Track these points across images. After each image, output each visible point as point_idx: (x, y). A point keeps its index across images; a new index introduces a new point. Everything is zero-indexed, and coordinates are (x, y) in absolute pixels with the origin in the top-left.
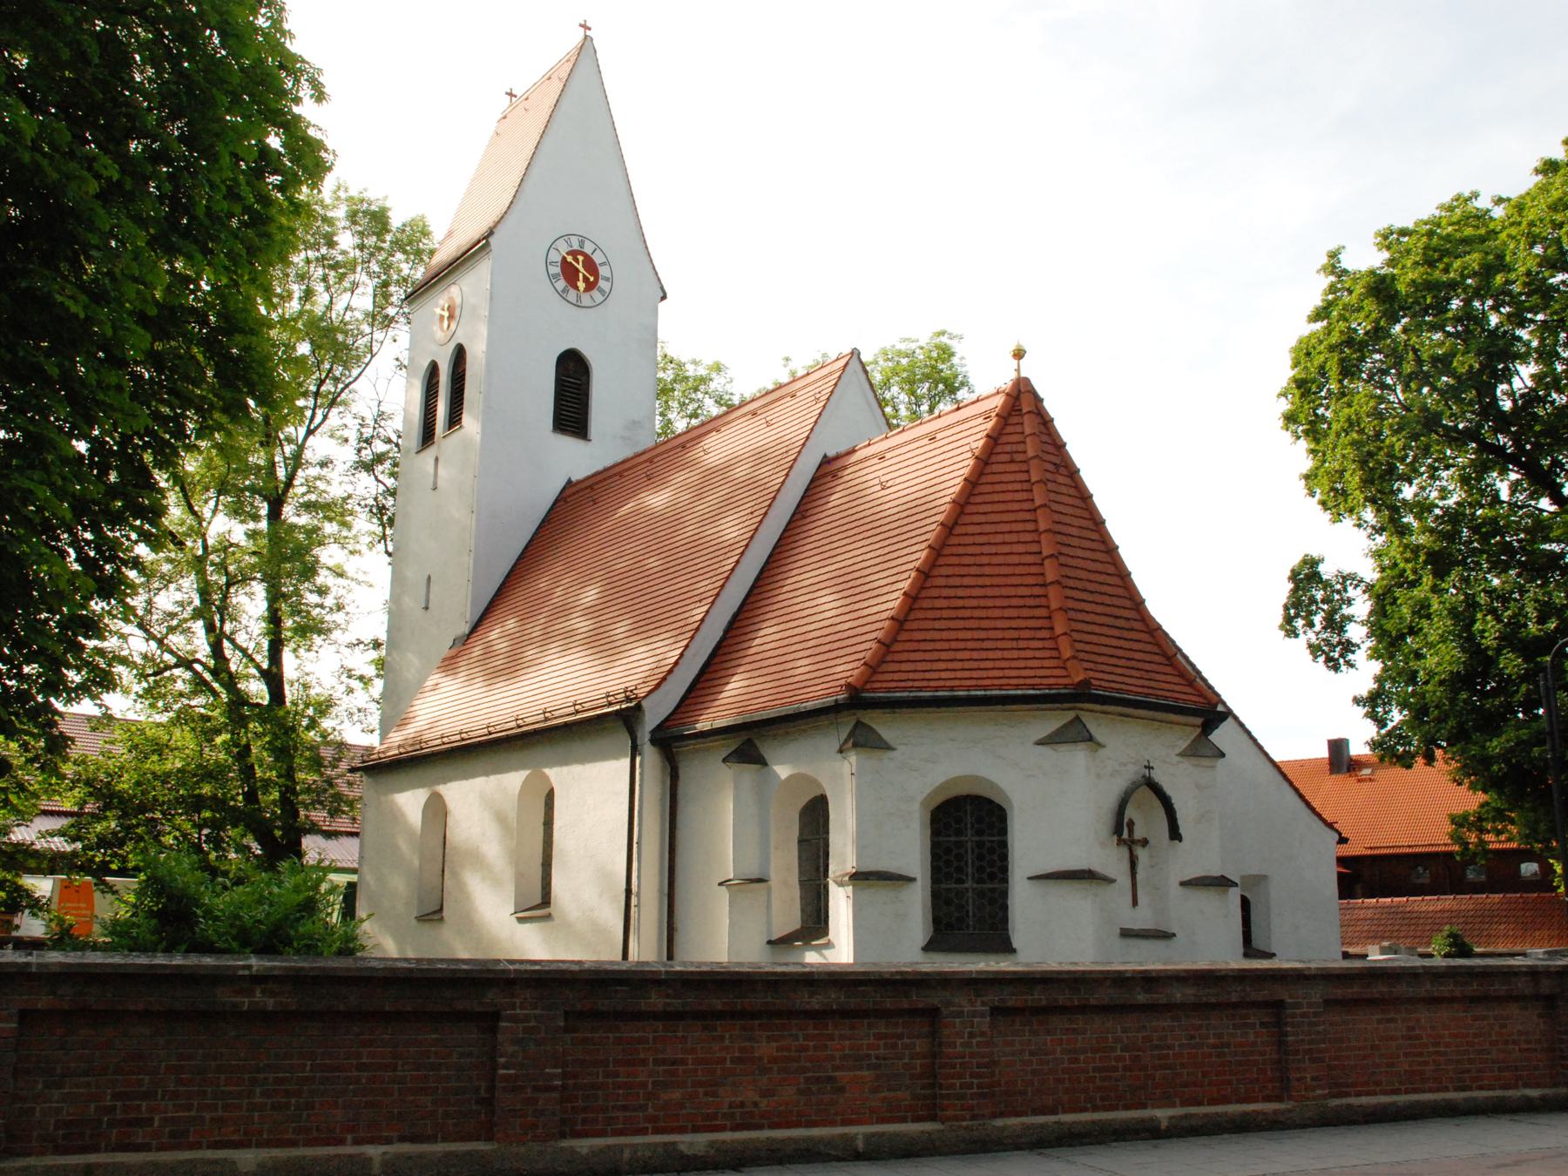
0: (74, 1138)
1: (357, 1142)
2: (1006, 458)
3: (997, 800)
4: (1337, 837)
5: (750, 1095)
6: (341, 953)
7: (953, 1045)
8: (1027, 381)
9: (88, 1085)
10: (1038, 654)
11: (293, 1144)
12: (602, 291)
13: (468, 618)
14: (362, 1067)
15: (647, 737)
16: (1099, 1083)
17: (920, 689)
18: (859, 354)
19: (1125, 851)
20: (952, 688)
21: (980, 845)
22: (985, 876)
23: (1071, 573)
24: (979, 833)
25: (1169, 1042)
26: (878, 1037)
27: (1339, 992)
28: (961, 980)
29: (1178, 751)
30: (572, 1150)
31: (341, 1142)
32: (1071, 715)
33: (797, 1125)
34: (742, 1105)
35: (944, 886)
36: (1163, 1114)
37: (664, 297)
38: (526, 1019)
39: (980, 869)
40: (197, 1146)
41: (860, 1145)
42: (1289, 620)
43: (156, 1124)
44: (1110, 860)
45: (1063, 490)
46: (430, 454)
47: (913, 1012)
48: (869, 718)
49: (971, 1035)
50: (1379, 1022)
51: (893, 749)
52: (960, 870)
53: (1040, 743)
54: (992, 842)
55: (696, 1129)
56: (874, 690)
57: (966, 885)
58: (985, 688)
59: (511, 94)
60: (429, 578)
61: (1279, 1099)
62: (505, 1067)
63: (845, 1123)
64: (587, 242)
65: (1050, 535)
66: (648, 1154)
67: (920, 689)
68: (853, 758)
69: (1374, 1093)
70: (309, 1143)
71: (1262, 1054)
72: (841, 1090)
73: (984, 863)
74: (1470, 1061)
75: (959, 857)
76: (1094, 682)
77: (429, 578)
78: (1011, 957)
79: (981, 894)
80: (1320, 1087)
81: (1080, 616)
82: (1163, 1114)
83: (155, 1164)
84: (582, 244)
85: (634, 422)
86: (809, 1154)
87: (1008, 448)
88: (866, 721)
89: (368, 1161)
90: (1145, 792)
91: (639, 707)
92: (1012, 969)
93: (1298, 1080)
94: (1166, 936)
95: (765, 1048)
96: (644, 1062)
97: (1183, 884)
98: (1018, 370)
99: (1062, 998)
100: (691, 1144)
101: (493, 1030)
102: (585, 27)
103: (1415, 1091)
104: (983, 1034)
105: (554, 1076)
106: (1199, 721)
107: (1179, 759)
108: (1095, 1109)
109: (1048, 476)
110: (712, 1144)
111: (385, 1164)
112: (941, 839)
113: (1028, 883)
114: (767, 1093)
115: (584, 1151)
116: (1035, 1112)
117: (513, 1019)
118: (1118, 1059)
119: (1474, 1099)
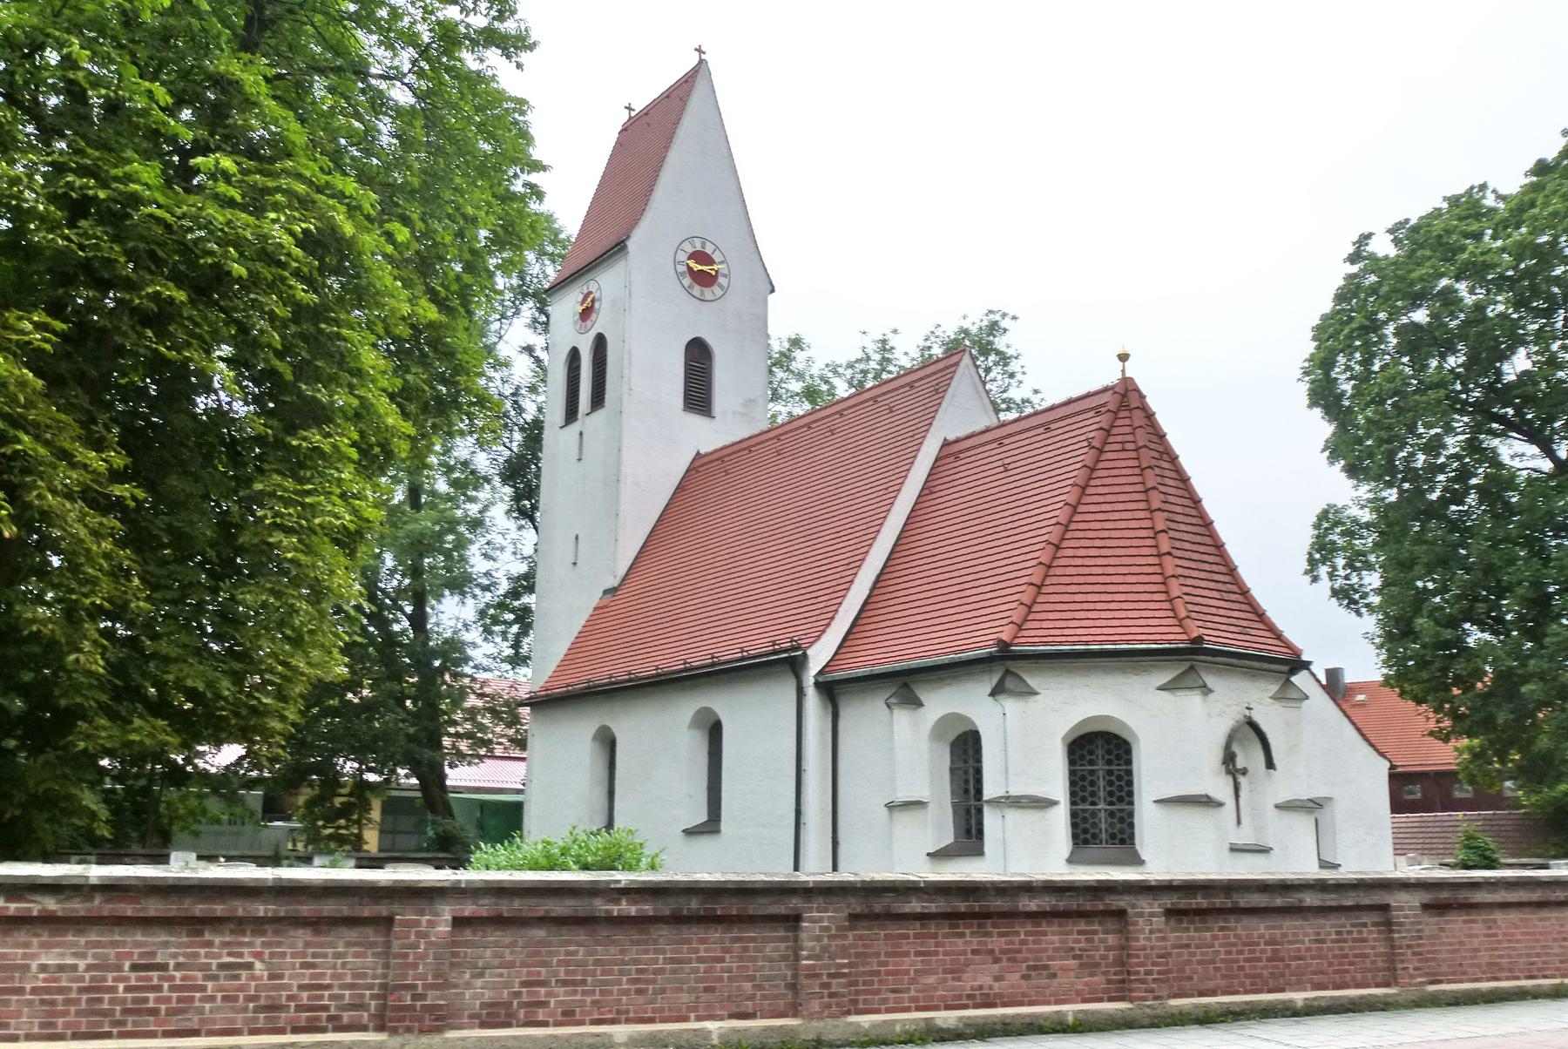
0: (495, 1016)
1: (699, 1019)
2: (1119, 447)
3: (1124, 735)
4: (1388, 765)
5: (986, 980)
6: (653, 867)
7: (1137, 940)
8: (1131, 379)
9: (501, 975)
11: (651, 1020)
12: (721, 286)
14: (700, 960)
15: (811, 681)
16: (1248, 971)
17: (1060, 643)
19: (1230, 779)
20: (1087, 643)
21: (1110, 773)
22: (1114, 799)
23: (1178, 544)
25: (1301, 938)
26: (1079, 933)
29: (1271, 694)
30: (858, 1024)
31: (686, 1019)
32: (1186, 665)
33: (1021, 1004)
34: (981, 988)
35: (1081, 807)
36: (1298, 997)
37: (773, 291)
38: (821, 920)
39: (1111, 794)
40: (581, 1023)
41: (1070, 1019)
42: (1313, 563)
43: (552, 1005)
44: (1219, 787)
45: (1167, 473)
46: (575, 428)
48: (1014, 666)
49: (1151, 932)
50: (1465, 922)
52: (1093, 794)
53: (1161, 688)
55: (948, 1008)
58: (1114, 642)
59: (629, 108)
60: (577, 537)
61: (1387, 985)
62: (807, 958)
63: (1058, 1002)
64: (708, 244)
66: (913, 1027)
69: (1461, 981)
70: (664, 1020)
71: (1373, 948)
72: (1054, 976)
73: (1090, 789)
74: (1538, 955)
75: (1092, 783)
76: (1206, 638)
77: (577, 537)
78: (1140, 869)
79: (1112, 814)
80: (1420, 976)
81: (1189, 582)
82: (1298, 997)
83: (555, 1037)
84: (703, 245)
85: (750, 400)
86: (1008, 1030)
87: (1119, 439)
89: (706, 1034)
90: (1248, 729)
91: (805, 656)
92: (664, 879)
93: (1404, 969)
94: (1265, 850)
95: (996, 942)
96: (907, 954)
97: (1277, 807)
98: (1123, 371)
99: (1218, 901)
100: (945, 1019)
101: (796, 928)
102: (699, 50)
103: (1496, 979)
104: (1160, 931)
105: (844, 966)
106: (1285, 668)
108: (1246, 992)
109: (1154, 462)
110: (960, 1019)
111: (721, 1036)
112: (1124, 767)
113: (1154, 806)
114: (998, 979)
115: (867, 1026)
116: (1201, 994)
117: (812, 920)
118: (1263, 951)
119: (1539, 986)
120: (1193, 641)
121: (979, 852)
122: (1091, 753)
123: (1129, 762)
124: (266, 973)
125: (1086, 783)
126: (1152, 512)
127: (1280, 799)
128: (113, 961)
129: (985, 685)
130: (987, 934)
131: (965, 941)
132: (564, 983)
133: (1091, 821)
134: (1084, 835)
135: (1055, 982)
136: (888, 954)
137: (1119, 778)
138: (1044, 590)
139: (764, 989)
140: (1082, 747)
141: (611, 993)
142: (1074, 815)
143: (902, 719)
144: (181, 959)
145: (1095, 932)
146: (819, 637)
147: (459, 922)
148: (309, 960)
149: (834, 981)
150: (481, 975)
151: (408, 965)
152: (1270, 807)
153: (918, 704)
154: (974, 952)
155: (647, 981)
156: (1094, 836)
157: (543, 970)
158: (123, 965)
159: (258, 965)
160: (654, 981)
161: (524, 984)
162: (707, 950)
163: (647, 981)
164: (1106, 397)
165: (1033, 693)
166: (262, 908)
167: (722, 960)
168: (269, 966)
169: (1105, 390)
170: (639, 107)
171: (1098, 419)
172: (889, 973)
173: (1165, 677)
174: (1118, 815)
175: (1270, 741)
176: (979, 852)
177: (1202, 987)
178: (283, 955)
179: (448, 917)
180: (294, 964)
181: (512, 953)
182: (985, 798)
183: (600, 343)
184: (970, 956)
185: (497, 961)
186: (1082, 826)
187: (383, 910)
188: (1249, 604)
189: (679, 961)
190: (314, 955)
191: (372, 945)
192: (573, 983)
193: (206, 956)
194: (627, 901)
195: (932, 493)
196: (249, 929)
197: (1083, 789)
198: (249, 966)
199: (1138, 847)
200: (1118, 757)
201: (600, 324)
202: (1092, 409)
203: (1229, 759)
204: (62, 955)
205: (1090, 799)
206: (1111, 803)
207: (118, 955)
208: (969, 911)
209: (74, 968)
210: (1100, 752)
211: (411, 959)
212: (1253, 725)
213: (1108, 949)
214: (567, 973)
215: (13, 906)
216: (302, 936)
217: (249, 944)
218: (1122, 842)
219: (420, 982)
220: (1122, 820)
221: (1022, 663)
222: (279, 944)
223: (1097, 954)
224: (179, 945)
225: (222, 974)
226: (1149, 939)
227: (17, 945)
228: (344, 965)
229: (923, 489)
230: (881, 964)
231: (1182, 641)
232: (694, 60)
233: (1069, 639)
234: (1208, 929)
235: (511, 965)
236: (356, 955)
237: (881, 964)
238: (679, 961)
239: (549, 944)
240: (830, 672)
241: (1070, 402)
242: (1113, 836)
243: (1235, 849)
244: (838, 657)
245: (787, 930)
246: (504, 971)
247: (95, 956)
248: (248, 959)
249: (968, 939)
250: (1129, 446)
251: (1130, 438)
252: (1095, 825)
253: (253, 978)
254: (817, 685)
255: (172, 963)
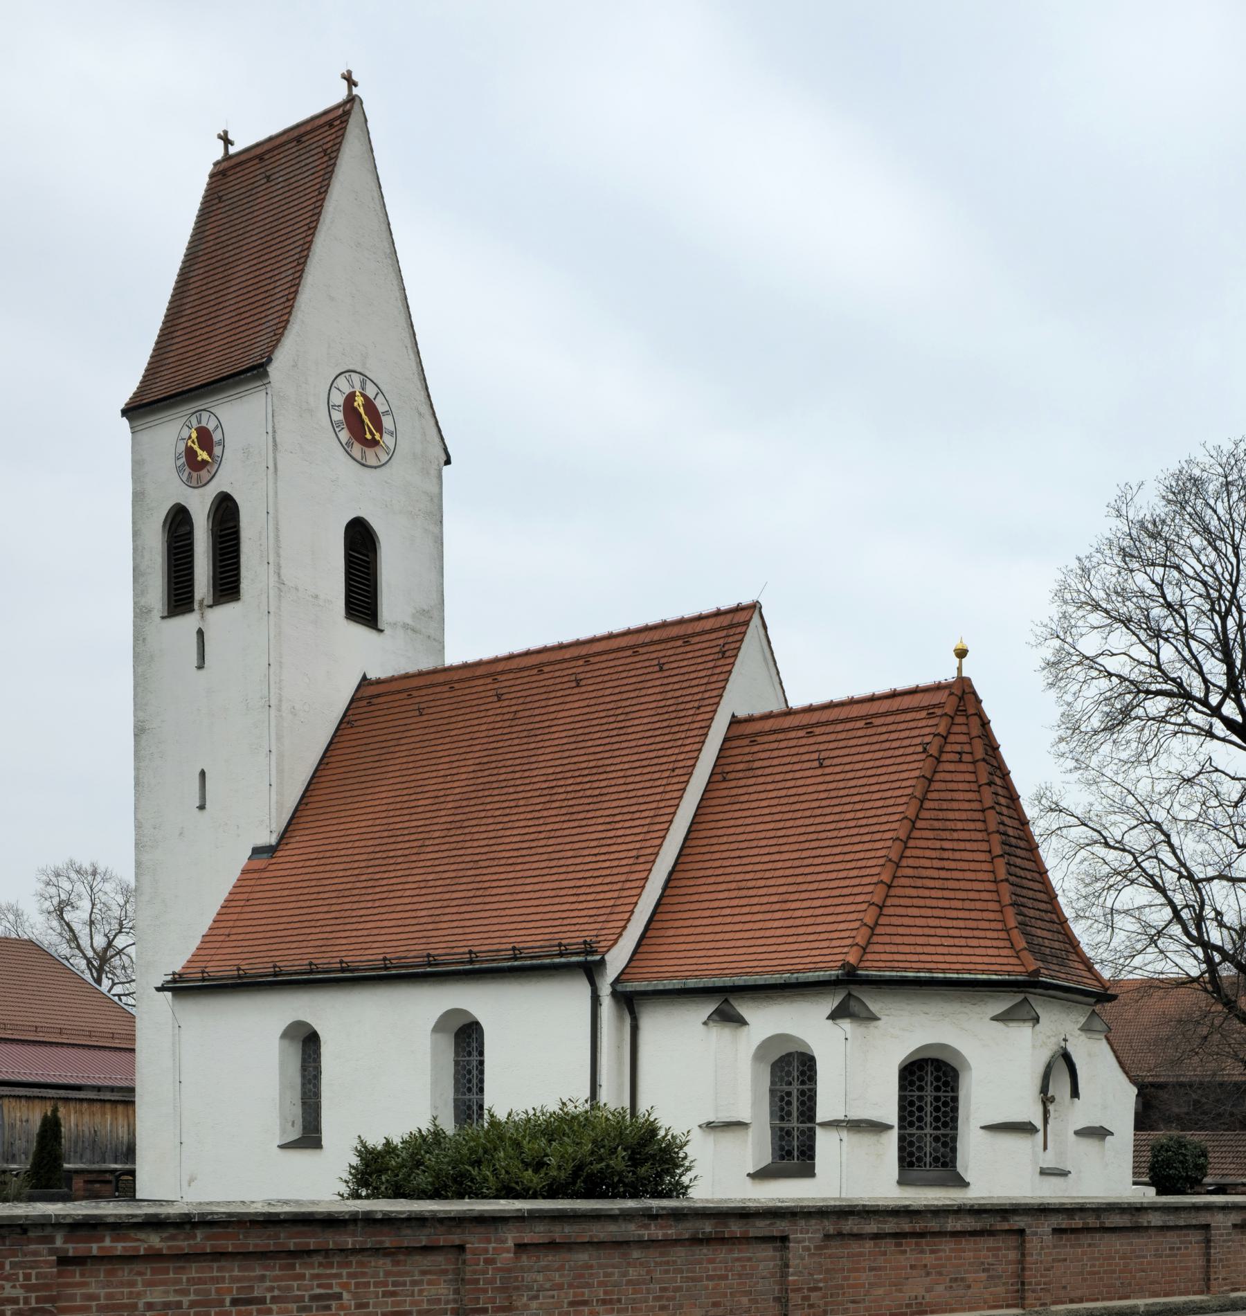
10: (995, 943)
12: (199, 478)
13: (274, 827)
14: (710, 1278)
17: (905, 969)
18: (761, 608)
20: (930, 971)
21: (937, 1099)
22: (940, 1124)
24: (937, 1089)
26: (989, 1249)
27: (1065, 1223)
28: (1024, 1209)
32: (1020, 997)
35: (942, 1132)
37: (448, 462)
38: (803, 1240)
39: (937, 1119)
46: (187, 624)
47: (1196, 1227)
48: (856, 991)
49: (1042, 1248)
51: (879, 1019)
52: (920, 1119)
53: (995, 1019)
54: (945, 1091)
56: (866, 968)
57: (925, 1131)
58: (958, 971)
59: (226, 140)
61: (1201, 1293)
62: (792, 1275)
65: (997, 835)
67: (905, 969)
68: (846, 1025)
72: (969, 1287)
73: (940, 1114)
75: (920, 1109)
79: (937, 1139)
80: (1226, 1285)
88: (855, 993)
94: (1064, 1174)
97: (1077, 1133)
98: (960, 669)
99: (1092, 1222)
105: (820, 1281)
107: (1079, 1032)
112: (907, 1093)
114: (929, 1290)
116: (1072, 1301)
120: (1030, 974)
121: (808, 1171)
122: (921, 1079)
123: (955, 1089)
124: (353, 1302)
125: (914, 1109)
126: (989, 834)
127: (1079, 1127)
128: (213, 1296)
129: (829, 1003)
130: (922, 1252)
131: (910, 1255)
132: (604, 1302)
133: (917, 1144)
134: (909, 1161)
135: (970, 1292)
136: (850, 1270)
137: (945, 1104)
138: (886, 911)
139: (757, 1303)
140: (912, 1073)
141: (641, 1310)
142: (902, 1139)
143: (721, 1035)
144: (276, 1293)
145: (999, 1249)
146: (616, 941)
147: (521, 1247)
148: (390, 1288)
149: (813, 1294)
150: (536, 1297)
151: (479, 1290)
152: (1071, 1133)
153: (742, 1022)
154: (912, 1267)
155: (668, 1299)
156: (919, 1159)
157: (586, 1291)
158: (224, 1300)
159: (345, 1295)
160: (674, 1299)
161: (572, 1304)
162: (714, 1270)
163: (668, 1299)
164: (941, 697)
165: (874, 1018)
166: (350, 1240)
167: (725, 1277)
168: (355, 1296)
169: (938, 687)
170: (241, 142)
171: (931, 722)
172: (849, 1286)
173: (1000, 1007)
174: (943, 1139)
175: (1077, 1067)
176: (808, 1171)
177: (1073, 1295)
178: (367, 1285)
179: (510, 1244)
180: (413, 1292)
181: (561, 1276)
182: (818, 1120)
183: (226, 511)
184: (909, 1271)
185: (548, 1285)
186: (908, 1149)
187: (456, 1239)
188: (1066, 934)
189: (693, 1280)
190: (395, 1284)
191: (445, 1272)
192: (611, 1302)
193: (298, 1289)
194: (656, 1226)
195: (724, 780)
196: (336, 1259)
197: (911, 1114)
198: (339, 1297)
199: (960, 1169)
200: (946, 1084)
201: (226, 480)
202: (923, 708)
203: (1044, 1089)
204: (167, 1293)
205: (917, 1124)
206: (937, 1128)
207: (218, 1291)
208: (911, 1230)
209: (179, 1305)
210: (929, 1078)
211: (481, 1285)
212: (1066, 1057)
213: (1009, 1263)
214: (606, 1293)
215: (120, 1245)
216: (385, 1264)
217: (338, 1276)
218: (945, 1165)
219: (490, 1305)
220: (945, 1145)
221: (865, 988)
222: (364, 1274)
223: (1000, 1268)
224: (275, 1279)
225: (314, 1305)
226: (1040, 1254)
227: (122, 1284)
228: (421, 1291)
229: (712, 774)
230: (845, 1278)
231: (1021, 973)
232: (338, 93)
233: (914, 965)
234: (1080, 1246)
235: (560, 1287)
236: (430, 1283)
237: (845, 1278)
238: (693, 1280)
239: (591, 1267)
240: (628, 980)
241: (894, 695)
242: (936, 1160)
243: (1044, 1172)
244: (633, 964)
245: (775, 1249)
246: (555, 1293)
247: (197, 1292)
248: (336, 1290)
249: (908, 1255)
250: (966, 758)
251: (967, 748)
252: (920, 1149)
253: (342, 1307)
254: (615, 994)
255: (268, 1295)
